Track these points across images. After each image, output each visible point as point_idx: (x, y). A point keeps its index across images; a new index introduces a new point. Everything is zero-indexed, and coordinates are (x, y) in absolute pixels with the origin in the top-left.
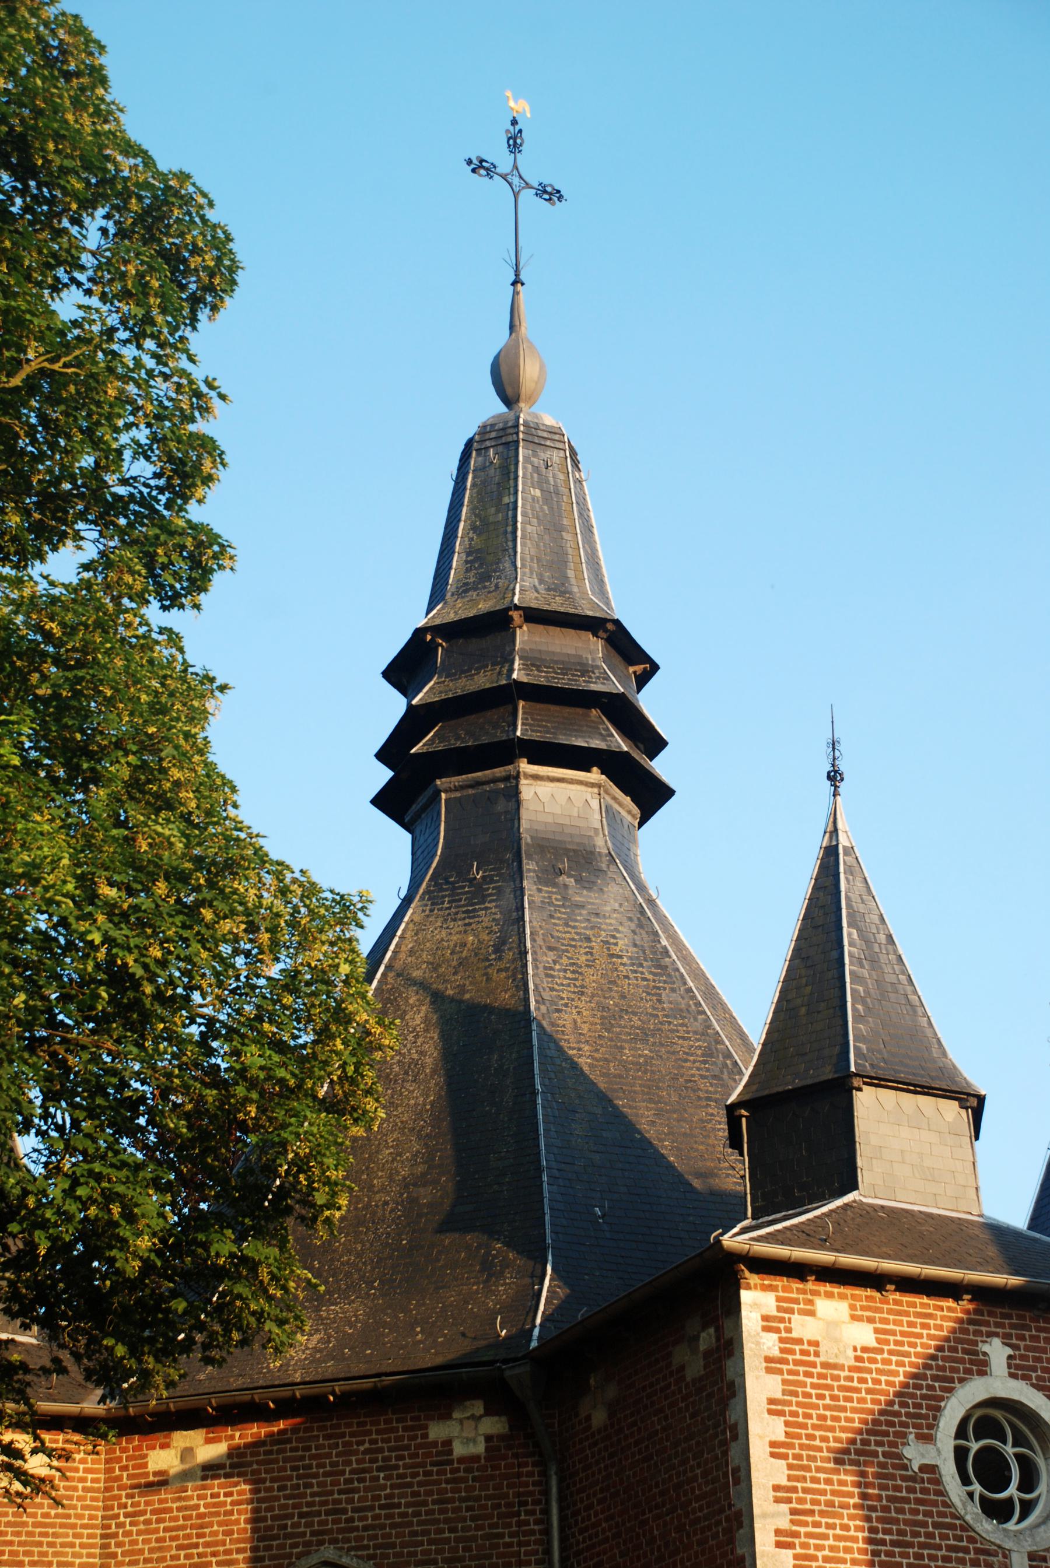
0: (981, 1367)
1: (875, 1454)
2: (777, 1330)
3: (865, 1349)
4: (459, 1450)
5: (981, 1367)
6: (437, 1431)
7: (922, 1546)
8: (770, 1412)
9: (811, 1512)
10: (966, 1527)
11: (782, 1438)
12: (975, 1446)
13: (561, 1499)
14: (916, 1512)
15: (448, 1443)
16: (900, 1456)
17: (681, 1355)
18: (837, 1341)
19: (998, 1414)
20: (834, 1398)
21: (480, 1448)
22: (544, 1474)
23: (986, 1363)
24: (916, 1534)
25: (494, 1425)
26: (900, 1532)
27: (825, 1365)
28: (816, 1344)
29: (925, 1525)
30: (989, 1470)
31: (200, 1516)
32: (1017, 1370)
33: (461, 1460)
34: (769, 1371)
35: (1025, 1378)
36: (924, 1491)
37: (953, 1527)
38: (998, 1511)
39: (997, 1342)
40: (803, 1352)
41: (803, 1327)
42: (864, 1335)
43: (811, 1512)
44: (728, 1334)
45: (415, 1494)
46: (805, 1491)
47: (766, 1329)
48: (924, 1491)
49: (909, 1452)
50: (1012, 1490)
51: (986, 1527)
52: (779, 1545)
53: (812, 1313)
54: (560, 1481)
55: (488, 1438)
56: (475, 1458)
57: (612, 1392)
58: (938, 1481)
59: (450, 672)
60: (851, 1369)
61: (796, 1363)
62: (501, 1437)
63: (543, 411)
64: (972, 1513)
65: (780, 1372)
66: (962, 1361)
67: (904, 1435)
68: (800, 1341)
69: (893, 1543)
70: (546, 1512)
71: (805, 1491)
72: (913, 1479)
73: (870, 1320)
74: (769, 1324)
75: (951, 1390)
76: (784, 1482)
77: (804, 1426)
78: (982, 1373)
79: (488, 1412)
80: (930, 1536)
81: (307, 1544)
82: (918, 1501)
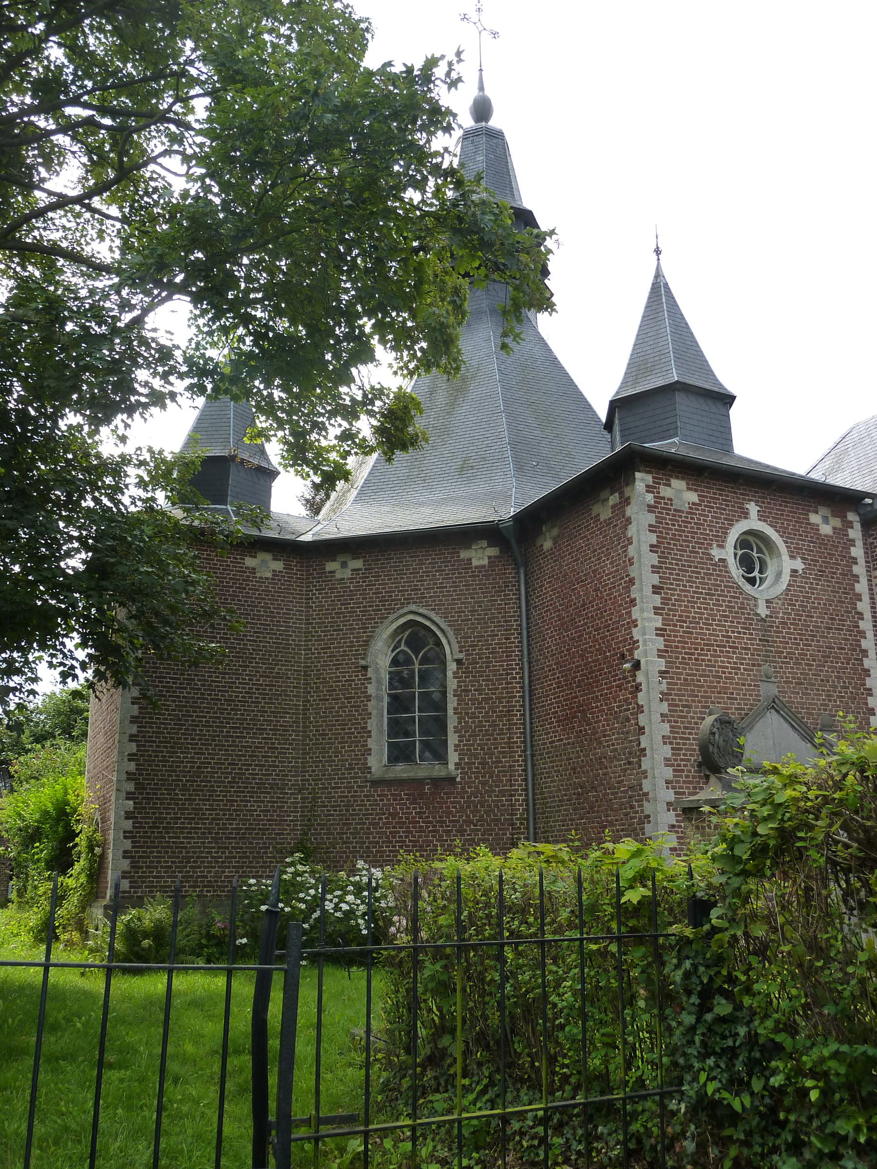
0: (746, 515)
1: (698, 553)
2: (653, 492)
3: (693, 504)
4: (475, 563)
5: (746, 515)
6: (464, 554)
7: (719, 595)
8: (650, 531)
9: (669, 579)
10: (739, 587)
11: (655, 543)
12: (740, 552)
13: (526, 584)
14: (716, 580)
15: (470, 559)
16: (709, 554)
17: (596, 509)
18: (681, 499)
19: (751, 539)
20: (679, 526)
21: (485, 562)
22: (518, 573)
23: (747, 513)
24: (717, 590)
25: (493, 551)
26: (709, 589)
27: (675, 510)
28: (671, 500)
29: (720, 586)
30: (746, 563)
31: (351, 591)
32: (762, 517)
33: (476, 567)
34: (649, 511)
35: (765, 521)
36: (720, 571)
37: (732, 587)
38: (752, 581)
39: (753, 503)
40: (665, 504)
41: (666, 492)
42: (693, 497)
43: (669, 579)
44: (627, 495)
45: (454, 582)
46: (666, 568)
47: (647, 491)
48: (720, 571)
49: (713, 552)
50: (756, 573)
51: (747, 587)
52: (654, 593)
53: (669, 485)
54: (526, 575)
55: (489, 557)
56: (484, 566)
57: (555, 532)
58: (726, 567)
59: (370, 491)
60: (688, 513)
61: (662, 508)
62: (495, 557)
63: (488, 92)
64: (742, 582)
65: (654, 512)
66: (736, 512)
67: (711, 545)
68: (663, 498)
69: (706, 594)
70: (519, 590)
71: (666, 568)
72: (715, 565)
73: (696, 490)
74: (649, 489)
75: (732, 525)
76: (656, 564)
77: (665, 538)
78: (746, 518)
79: (489, 546)
80: (723, 591)
81: (403, 604)
82: (718, 575)
